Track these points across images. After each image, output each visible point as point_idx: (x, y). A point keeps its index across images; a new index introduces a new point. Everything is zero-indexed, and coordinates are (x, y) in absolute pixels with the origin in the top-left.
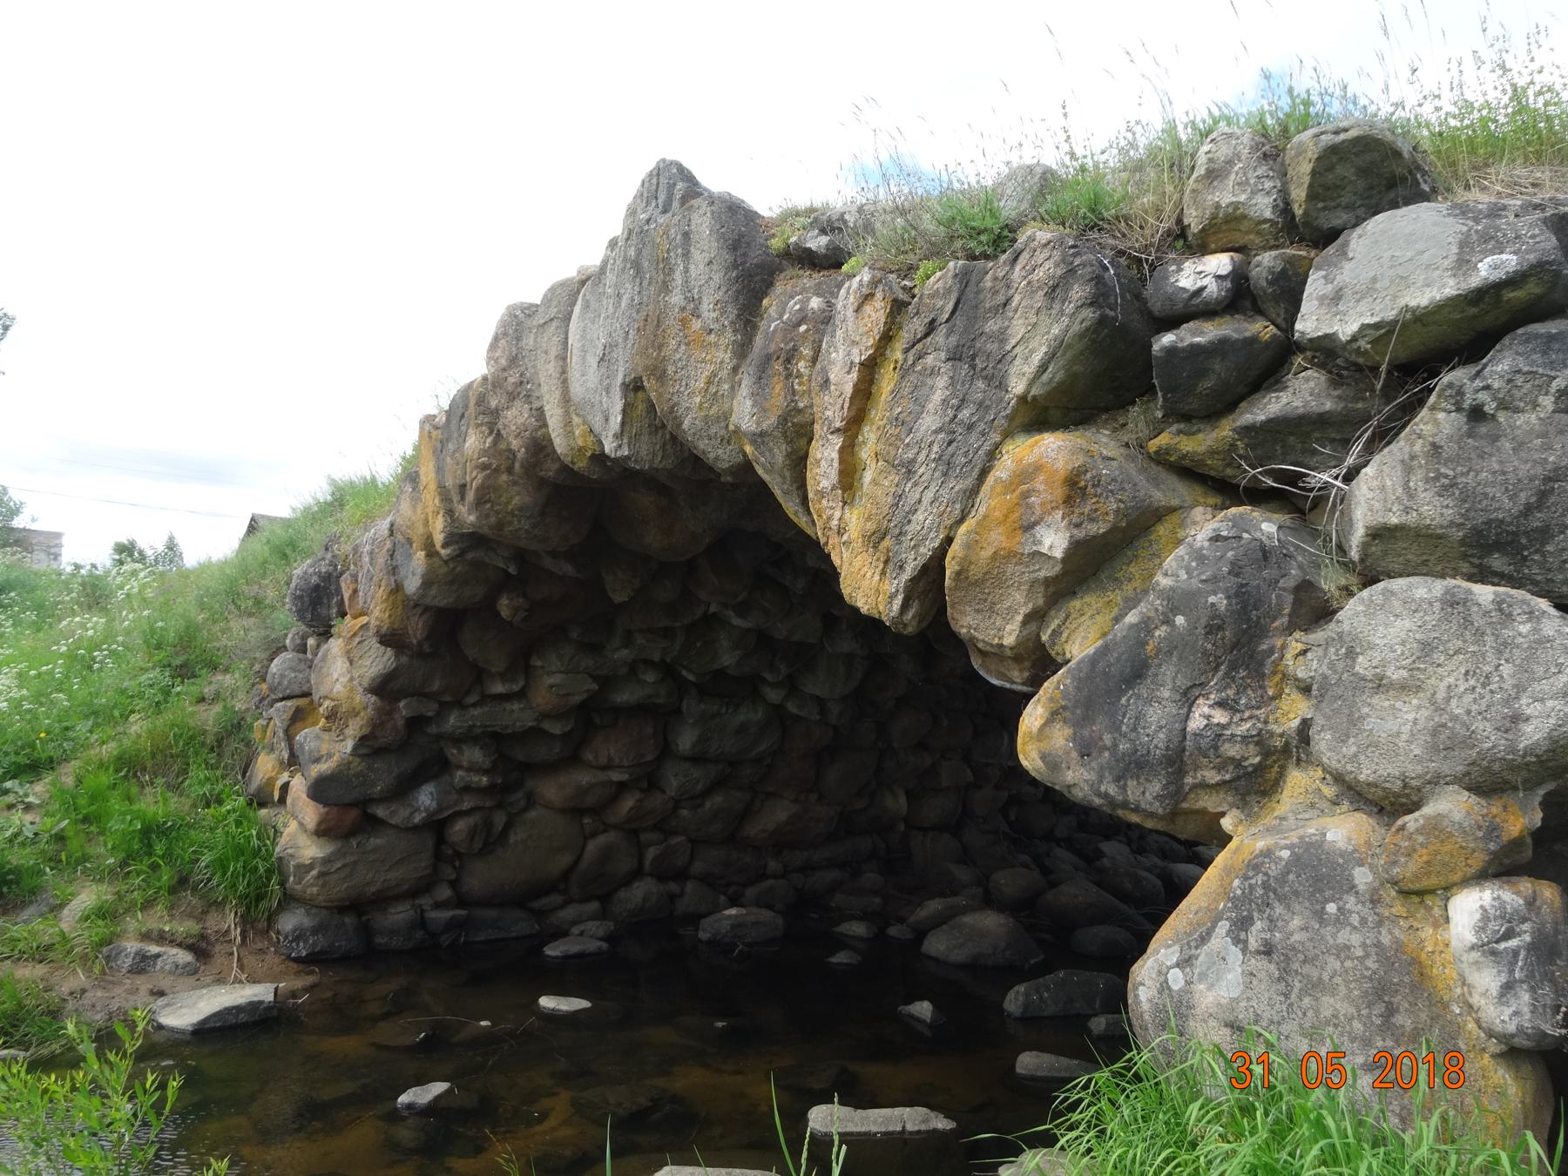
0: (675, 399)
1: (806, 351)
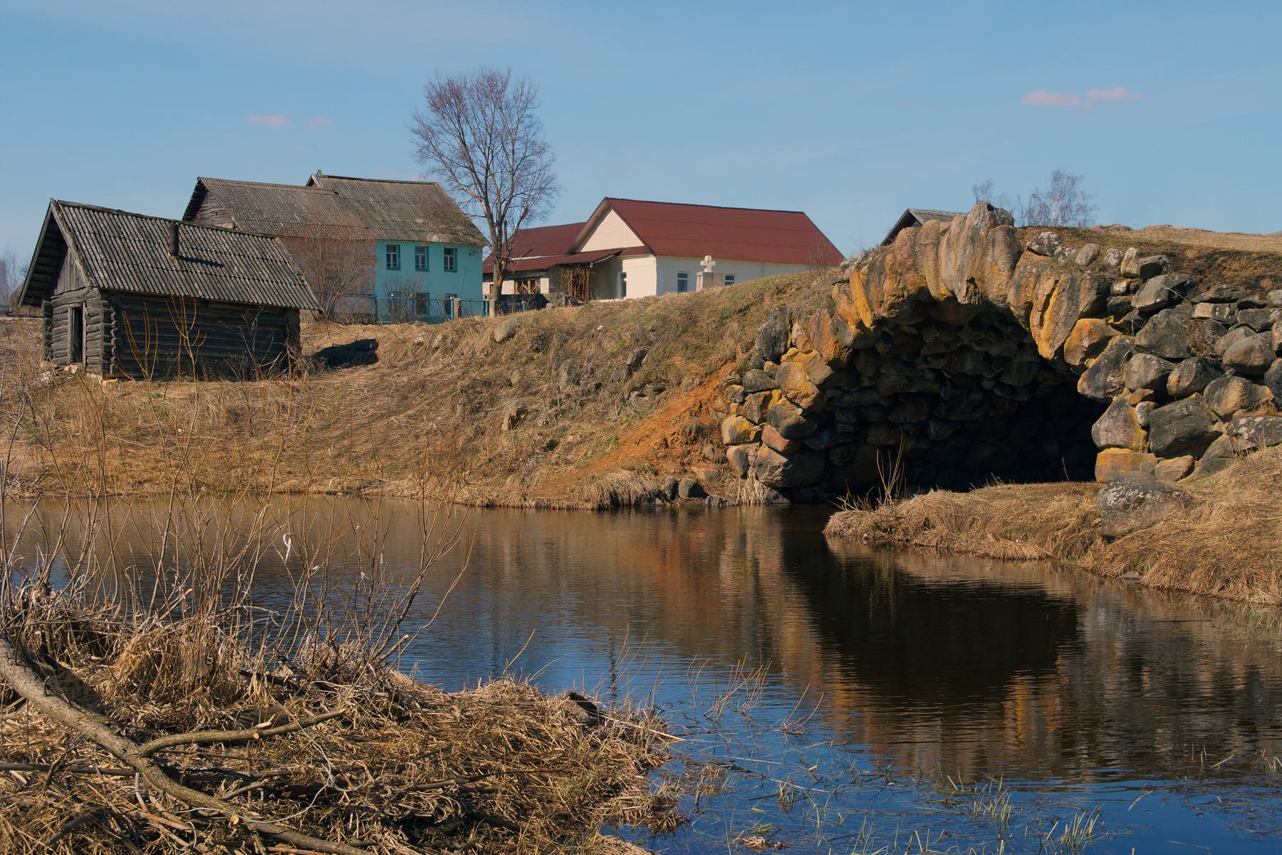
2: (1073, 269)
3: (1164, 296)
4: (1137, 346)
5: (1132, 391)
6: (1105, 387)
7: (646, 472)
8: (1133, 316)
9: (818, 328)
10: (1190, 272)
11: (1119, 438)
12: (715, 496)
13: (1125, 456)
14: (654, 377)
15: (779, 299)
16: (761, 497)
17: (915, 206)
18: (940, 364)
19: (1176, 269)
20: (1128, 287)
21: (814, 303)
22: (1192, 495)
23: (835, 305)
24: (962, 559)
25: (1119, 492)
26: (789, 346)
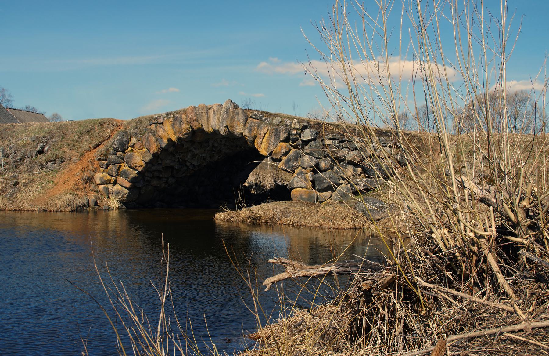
13: (305, 191)
15: (101, 128)
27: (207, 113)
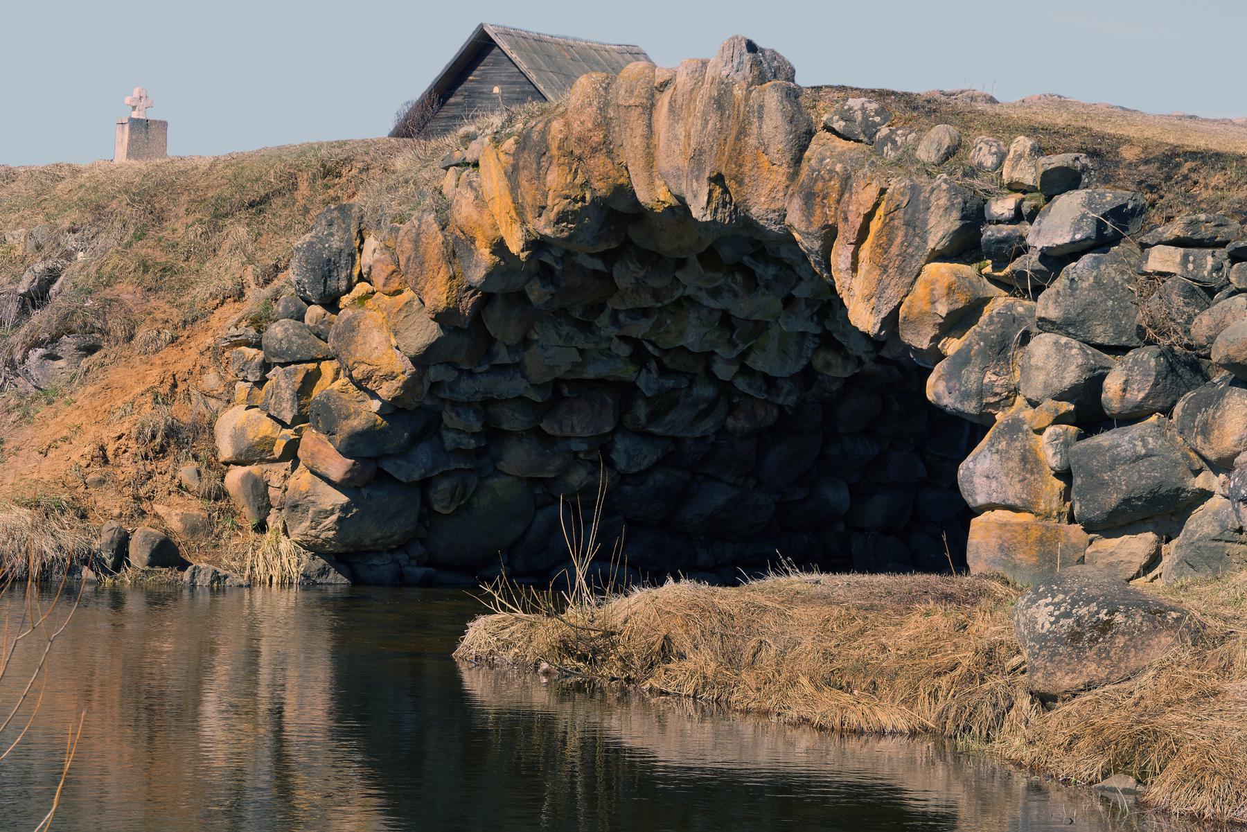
0: (748, 196)
1: (834, 196)
2: (913, 170)
3: (1087, 230)
4: (1041, 319)
5: (1033, 404)
6: (980, 393)
7: (63, 512)
8: (1029, 263)
9: (416, 249)
10: (1133, 187)
11: (1013, 492)
12: (203, 565)
13: (1026, 527)
14: (79, 322)
15: (327, 187)
16: (295, 572)
17: (494, 22)
18: (640, 329)
19: (1106, 180)
20: (1018, 209)
21: (406, 200)
22: (1203, 619)
23: (449, 206)
24: (747, 727)
25: (1057, 605)
26: (355, 279)
27: (649, 109)
